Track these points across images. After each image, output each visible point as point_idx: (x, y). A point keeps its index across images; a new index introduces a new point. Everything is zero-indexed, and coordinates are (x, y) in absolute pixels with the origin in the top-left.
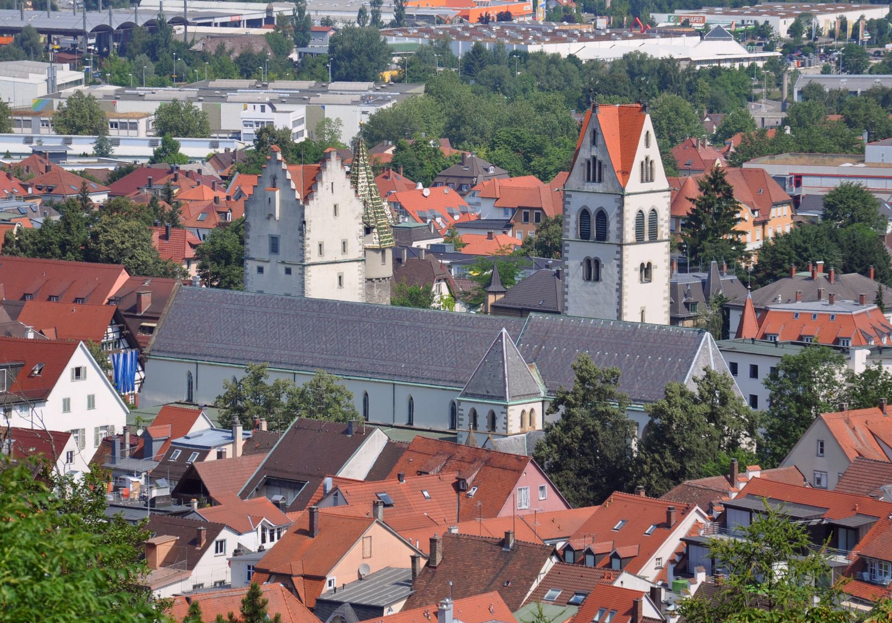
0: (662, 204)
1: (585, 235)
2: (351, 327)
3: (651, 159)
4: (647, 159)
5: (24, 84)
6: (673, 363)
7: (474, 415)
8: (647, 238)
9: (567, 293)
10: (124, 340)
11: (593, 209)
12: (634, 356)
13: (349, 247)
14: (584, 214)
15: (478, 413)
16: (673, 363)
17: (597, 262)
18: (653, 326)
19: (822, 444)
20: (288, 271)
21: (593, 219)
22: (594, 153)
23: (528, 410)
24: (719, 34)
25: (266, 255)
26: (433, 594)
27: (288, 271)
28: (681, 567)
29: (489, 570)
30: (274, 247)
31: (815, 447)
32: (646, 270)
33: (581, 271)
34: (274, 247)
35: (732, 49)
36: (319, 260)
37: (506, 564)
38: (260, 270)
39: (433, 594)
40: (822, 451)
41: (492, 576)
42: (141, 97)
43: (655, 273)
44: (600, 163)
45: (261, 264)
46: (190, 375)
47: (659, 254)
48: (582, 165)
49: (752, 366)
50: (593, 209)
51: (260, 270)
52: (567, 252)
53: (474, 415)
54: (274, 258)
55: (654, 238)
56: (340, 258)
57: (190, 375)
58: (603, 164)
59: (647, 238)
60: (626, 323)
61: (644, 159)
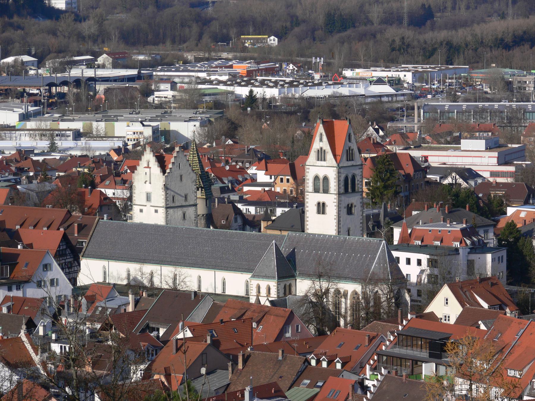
0: (332, 174)
1: (316, 190)
2: (191, 241)
3: (352, 148)
4: (349, 148)
5: (8, 116)
6: (366, 257)
7: (259, 287)
8: (350, 190)
9: (361, 223)
10: (68, 249)
11: (321, 177)
12: (345, 254)
13: (189, 198)
14: (316, 178)
15: (261, 286)
16: (366, 257)
17: (324, 204)
18: (314, 235)
19: (447, 300)
20: (156, 211)
21: (321, 181)
22: (321, 146)
23: (288, 284)
24: (380, 81)
25: (144, 202)
26: (240, 383)
27: (156, 211)
28: (373, 367)
29: (271, 370)
30: (148, 198)
31: (443, 301)
32: (321, 208)
33: (315, 208)
34: (148, 198)
35: (387, 89)
36: (173, 205)
37: (280, 367)
38: (141, 211)
39: (240, 383)
40: (447, 303)
41: (272, 374)
42: (73, 120)
43: (327, 209)
44: (324, 151)
45: (156, 208)
46: (104, 267)
47: (331, 200)
48: (315, 152)
49: (407, 258)
50: (321, 177)
51: (141, 211)
52: (308, 199)
53: (259, 287)
54: (149, 204)
55: (326, 191)
56: (184, 204)
57: (104, 267)
58: (326, 151)
59: (350, 190)
60: (310, 234)
61: (348, 148)
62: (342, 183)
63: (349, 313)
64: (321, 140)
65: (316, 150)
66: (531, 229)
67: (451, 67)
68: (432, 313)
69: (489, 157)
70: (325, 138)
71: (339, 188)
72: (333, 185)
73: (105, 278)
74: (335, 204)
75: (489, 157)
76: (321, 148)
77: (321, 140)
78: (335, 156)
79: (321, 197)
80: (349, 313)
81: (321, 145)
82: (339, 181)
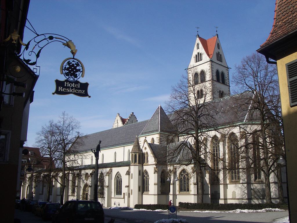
14: (196, 74)
44: (201, 54)
62: (215, 74)
63: (227, 157)
64: (198, 48)
65: (195, 56)
66: (30, 59)
67: (259, 210)
68: (9, 84)
69: (124, 203)
70: (201, 45)
71: (212, 76)
72: (208, 77)
73: (202, 201)
74: (209, 65)
75: (124, 203)
76: (198, 53)
77: (198, 48)
78: (208, 55)
79: (198, 87)
80: (227, 157)
81: (198, 51)
82: (212, 71)
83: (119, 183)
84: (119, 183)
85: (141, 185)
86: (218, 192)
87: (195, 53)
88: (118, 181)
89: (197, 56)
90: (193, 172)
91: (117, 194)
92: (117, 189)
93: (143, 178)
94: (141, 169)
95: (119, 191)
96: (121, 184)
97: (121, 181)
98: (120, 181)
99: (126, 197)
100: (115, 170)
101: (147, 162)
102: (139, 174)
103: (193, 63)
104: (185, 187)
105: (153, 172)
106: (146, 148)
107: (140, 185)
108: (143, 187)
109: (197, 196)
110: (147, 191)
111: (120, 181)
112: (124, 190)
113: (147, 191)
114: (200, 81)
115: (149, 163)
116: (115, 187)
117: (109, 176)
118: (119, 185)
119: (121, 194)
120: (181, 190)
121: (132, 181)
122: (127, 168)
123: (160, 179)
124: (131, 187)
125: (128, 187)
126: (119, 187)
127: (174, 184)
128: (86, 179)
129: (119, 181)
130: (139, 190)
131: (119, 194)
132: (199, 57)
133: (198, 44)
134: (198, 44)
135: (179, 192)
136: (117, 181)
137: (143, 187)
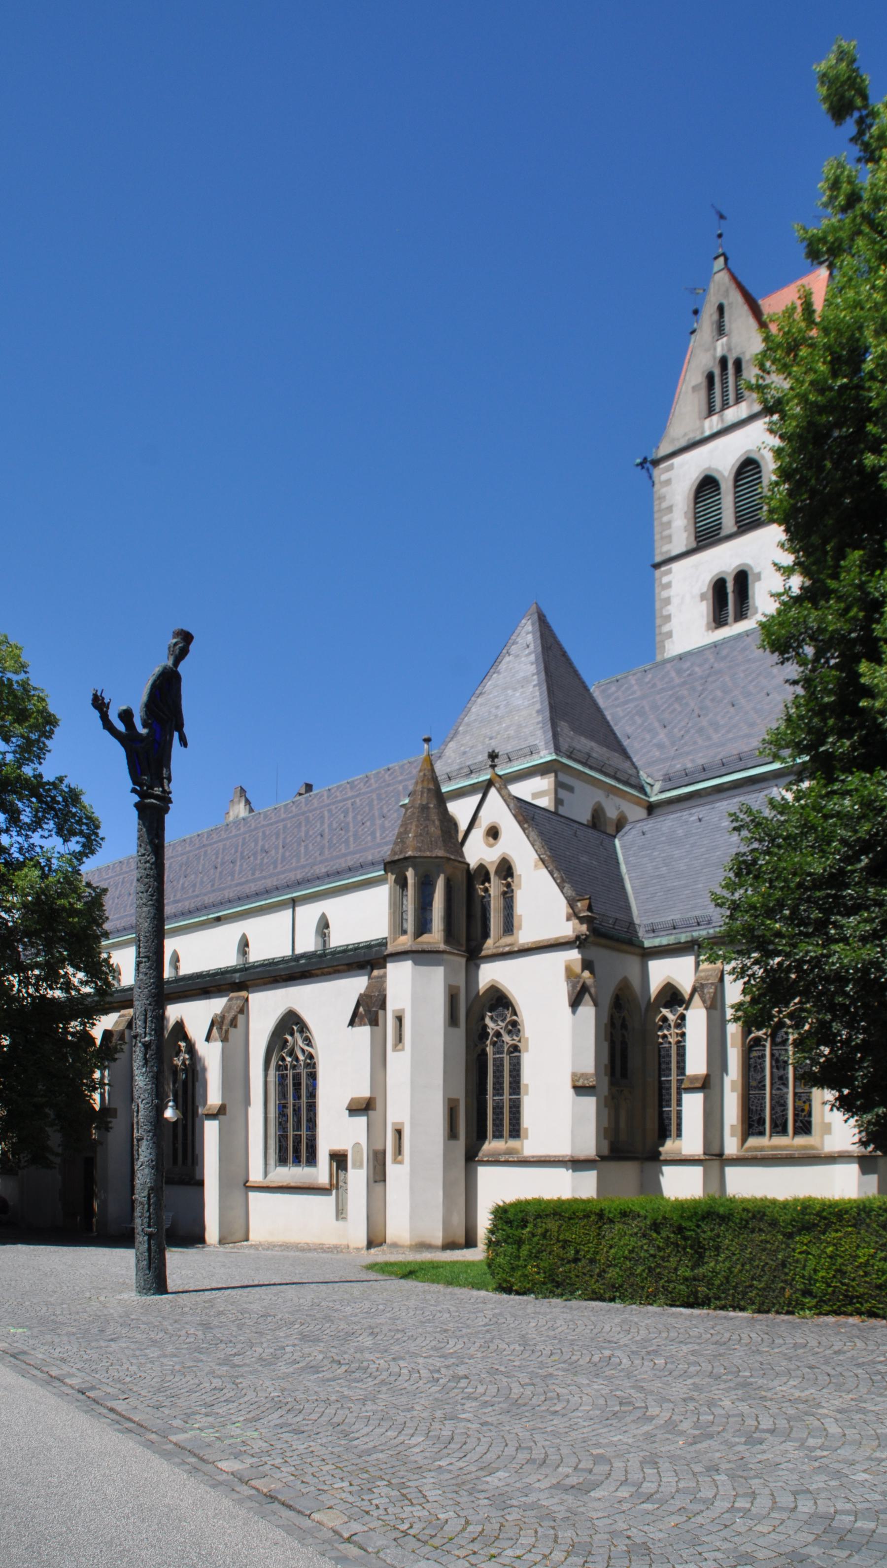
1: (707, 536)
14: (707, 485)
64: (721, 330)
76: (723, 361)
77: (721, 330)
83: (297, 1085)
84: (297, 1085)
85: (460, 1094)
86: (198, 1178)
87: (701, 356)
88: (290, 1073)
89: (710, 377)
90: (736, 1019)
91: (282, 1160)
92: (282, 1125)
93: (483, 1039)
94: (461, 982)
95: (295, 1140)
96: (312, 1095)
97: (313, 1076)
98: (304, 1072)
99: (357, 1178)
100: (266, 1008)
101: (509, 927)
102: (452, 1019)
103: (686, 414)
104: (779, 1103)
105: (562, 992)
106: (493, 833)
107: (454, 1096)
108: (483, 1108)
109: (698, 1170)
110: (506, 1132)
111: (304, 1072)
112: (336, 1130)
113: (506, 1132)
114: (729, 522)
115: (525, 936)
116: (272, 1114)
117: (225, 1039)
118: (297, 1096)
119: (312, 1160)
120: (752, 1124)
121: (399, 1063)
122: (355, 986)
123: (606, 1046)
124: (398, 1109)
125: (362, 1108)
126: (297, 1111)
127: (707, 1085)
128: (30, 716)
129: (297, 1078)
130: (452, 1133)
131: (297, 1161)
132: (724, 382)
133: (721, 309)
134: (721, 309)
135: (744, 1141)
136: (282, 1079)
137: (483, 1108)
